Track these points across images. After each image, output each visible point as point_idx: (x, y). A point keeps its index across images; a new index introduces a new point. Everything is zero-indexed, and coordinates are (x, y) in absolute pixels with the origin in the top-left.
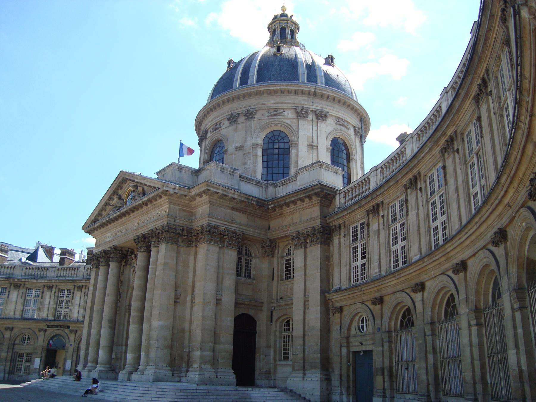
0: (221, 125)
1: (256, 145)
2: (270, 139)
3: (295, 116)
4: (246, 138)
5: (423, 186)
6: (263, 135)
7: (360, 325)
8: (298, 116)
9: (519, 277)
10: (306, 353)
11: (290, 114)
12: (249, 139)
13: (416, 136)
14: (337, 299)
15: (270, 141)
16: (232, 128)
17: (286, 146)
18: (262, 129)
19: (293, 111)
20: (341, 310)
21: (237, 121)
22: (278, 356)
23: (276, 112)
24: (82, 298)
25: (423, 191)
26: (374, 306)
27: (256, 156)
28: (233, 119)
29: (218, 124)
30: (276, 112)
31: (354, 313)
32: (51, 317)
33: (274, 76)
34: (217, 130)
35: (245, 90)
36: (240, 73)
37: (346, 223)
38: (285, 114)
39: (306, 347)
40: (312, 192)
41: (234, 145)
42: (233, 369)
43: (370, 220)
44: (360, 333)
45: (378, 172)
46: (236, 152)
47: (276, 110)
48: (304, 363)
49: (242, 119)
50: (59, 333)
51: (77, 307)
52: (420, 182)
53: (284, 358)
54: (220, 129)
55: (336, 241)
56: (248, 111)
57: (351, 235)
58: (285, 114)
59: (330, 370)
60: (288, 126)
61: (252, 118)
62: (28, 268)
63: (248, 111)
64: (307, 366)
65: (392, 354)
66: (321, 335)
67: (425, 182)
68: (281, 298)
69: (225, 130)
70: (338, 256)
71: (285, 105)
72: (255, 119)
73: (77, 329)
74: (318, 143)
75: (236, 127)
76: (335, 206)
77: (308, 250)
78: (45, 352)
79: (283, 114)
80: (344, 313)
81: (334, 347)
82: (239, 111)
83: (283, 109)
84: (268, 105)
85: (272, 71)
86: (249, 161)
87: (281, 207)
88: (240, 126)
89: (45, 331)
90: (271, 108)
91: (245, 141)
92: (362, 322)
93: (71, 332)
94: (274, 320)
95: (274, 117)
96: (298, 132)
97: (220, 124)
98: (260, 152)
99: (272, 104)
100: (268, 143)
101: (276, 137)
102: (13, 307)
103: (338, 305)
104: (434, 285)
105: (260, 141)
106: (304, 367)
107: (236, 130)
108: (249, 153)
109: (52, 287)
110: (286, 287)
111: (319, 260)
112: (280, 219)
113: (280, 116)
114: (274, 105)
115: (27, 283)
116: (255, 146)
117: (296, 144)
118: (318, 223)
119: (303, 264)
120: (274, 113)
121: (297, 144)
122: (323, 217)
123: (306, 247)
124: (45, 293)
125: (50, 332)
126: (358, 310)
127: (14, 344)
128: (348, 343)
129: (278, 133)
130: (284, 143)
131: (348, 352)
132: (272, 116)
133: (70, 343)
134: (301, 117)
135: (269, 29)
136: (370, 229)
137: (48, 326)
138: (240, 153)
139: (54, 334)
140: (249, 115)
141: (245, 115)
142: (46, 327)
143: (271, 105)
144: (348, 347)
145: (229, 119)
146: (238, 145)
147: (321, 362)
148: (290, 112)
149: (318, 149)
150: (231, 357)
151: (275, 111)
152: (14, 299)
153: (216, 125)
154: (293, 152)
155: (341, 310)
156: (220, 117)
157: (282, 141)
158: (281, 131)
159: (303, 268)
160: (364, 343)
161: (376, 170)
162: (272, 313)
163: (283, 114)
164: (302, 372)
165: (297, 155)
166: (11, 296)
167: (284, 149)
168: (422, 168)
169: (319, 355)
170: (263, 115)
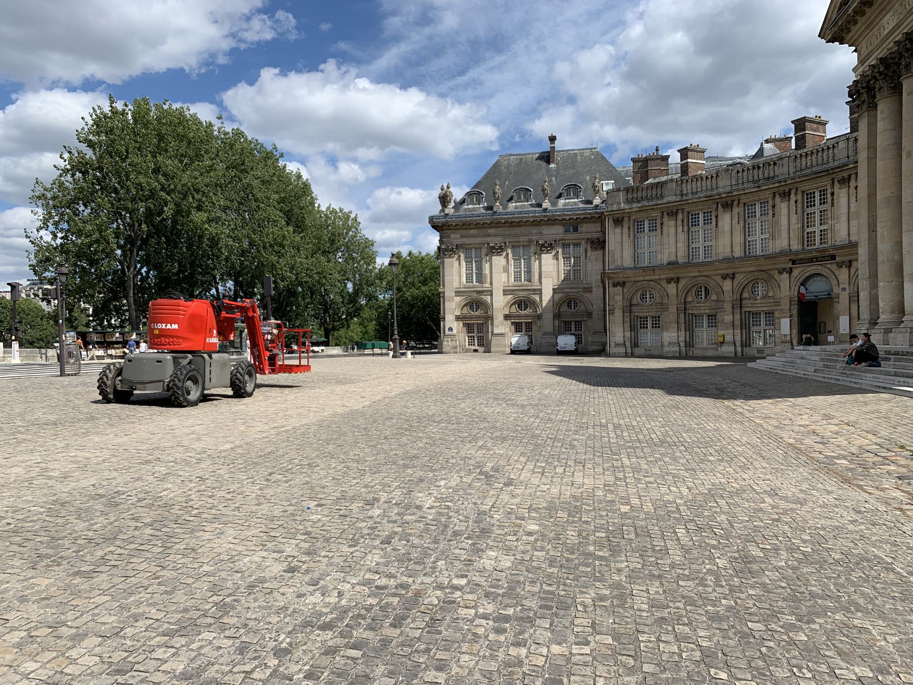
32: (795, 246)
51: (844, 218)
89: (790, 271)
93: (840, 266)
115: (743, 197)
137: (794, 262)
139: (808, 274)
152: (727, 228)
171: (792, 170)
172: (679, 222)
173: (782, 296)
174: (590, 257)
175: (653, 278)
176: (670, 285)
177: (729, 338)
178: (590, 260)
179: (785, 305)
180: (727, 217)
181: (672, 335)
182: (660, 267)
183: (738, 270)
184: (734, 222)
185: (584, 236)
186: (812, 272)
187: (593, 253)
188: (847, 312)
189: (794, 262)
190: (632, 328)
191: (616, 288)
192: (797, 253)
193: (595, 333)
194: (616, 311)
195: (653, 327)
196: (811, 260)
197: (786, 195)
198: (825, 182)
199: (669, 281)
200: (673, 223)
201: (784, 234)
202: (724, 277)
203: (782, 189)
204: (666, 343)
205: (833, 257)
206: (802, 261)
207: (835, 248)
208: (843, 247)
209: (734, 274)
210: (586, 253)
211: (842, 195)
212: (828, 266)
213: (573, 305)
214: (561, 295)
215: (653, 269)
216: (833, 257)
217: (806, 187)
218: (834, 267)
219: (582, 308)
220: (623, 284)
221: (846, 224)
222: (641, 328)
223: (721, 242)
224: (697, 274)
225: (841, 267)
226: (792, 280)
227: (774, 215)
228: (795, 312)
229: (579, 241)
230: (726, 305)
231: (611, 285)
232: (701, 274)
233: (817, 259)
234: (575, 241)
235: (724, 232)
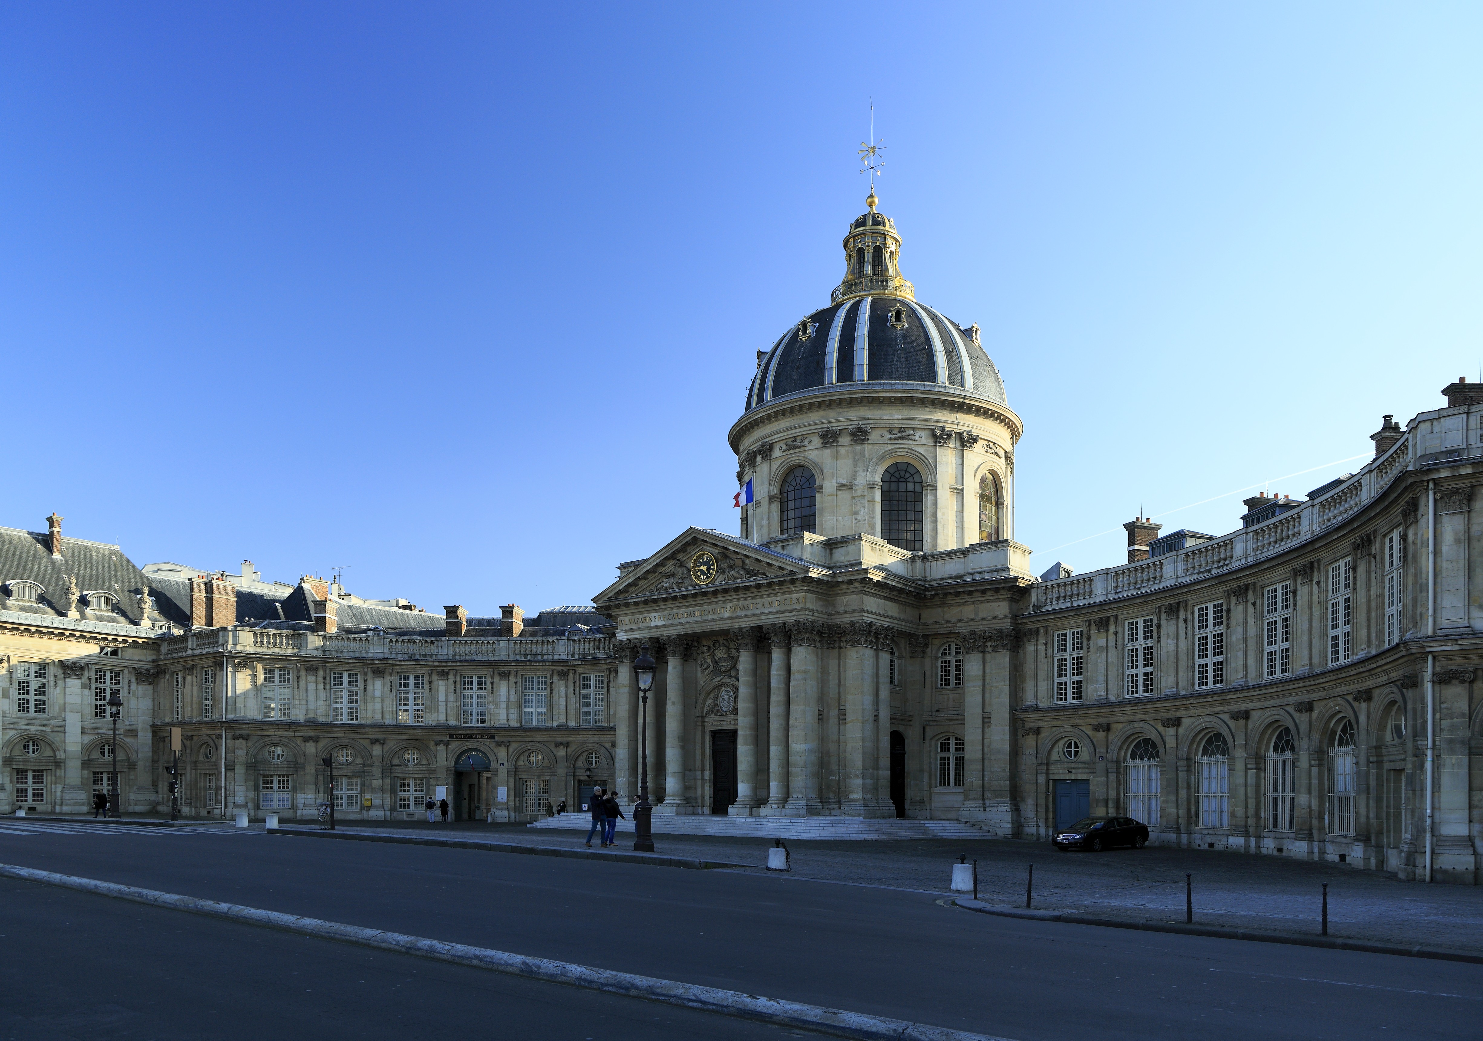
0: (806, 443)
1: (874, 484)
2: (892, 475)
3: (931, 442)
4: (856, 472)
5: (1189, 617)
6: (881, 469)
7: (1066, 750)
8: (935, 442)
9: (1321, 742)
10: (986, 779)
11: (923, 438)
12: (861, 474)
13: (1183, 556)
14: (1032, 720)
15: (893, 479)
16: (827, 452)
17: (918, 488)
18: (882, 458)
19: (927, 432)
20: (1037, 731)
21: (838, 442)
22: (933, 782)
23: (902, 434)
24: (512, 691)
25: (1189, 623)
26: (1094, 733)
27: (873, 501)
28: (829, 438)
29: (799, 439)
30: (902, 434)
31: (1059, 736)
32: (453, 722)
33: (897, 370)
34: (797, 450)
35: (846, 390)
36: (835, 354)
37: (1050, 629)
38: (917, 437)
39: (986, 773)
40: (1003, 585)
41: (834, 481)
42: (891, 798)
43: (1092, 632)
44: (1066, 760)
45: (1109, 576)
46: (840, 493)
47: (901, 430)
48: (983, 791)
49: (845, 440)
50: (475, 747)
51: (503, 705)
52: (1185, 611)
53: (941, 784)
54: (803, 449)
55: (1030, 648)
56: (859, 429)
57: (1056, 643)
58: (917, 437)
59: (1018, 799)
60: (921, 458)
61: (863, 440)
62: (394, 640)
63: (859, 429)
64: (988, 794)
65: (1120, 784)
66: (1010, 759)
67: (1193, 613)
68: (938, 711)
69: (815, 452)
70: (1033, 667)
71: (916, 422)
72: (869, 442)
73: (510, 739)
74: (963, 484)
75: (837, 452)
76: (1030, 603)
77: (988, 656)
78: (453, 776)
79: (913, 437)
80: (1042, 735)
81: (1027, 775)
82: (841, 425)
83: (913, 429)
84: (891, 422)
85: (893, 361)
86: (863, 510)
87: (946, 595)
88: (843, 451)
89: (447, 744)
90: (896, 425)
91: (854, 476)
92: (1070, 746)
93: (499, 744)
94: (928, 738)
95: (900, 442)
96: (936, 467)
97: (802, 441)
98: (878, 495)
99: (898, 419)
100: (890, 482)
101: (902, 473)
102: (378, 706)
103: (1033, 725)
104: (1196, 724)
105: (878, 479)
106: (983, 795)
107: (836, 456)
108: (863, 496)
109: (447, 674)
110: (946, 697)
111: (1008, 670)
112: (939, 610)
113: (909, 439)
114: (901, 422)
115: (398, 667)
116: (871, 485)
117: (933, 486)
118: (1006, 625)
119: (981, 673)
120: (900, 435)
121: (934, 487)
122: (1015, 617)
123: (985, 652)
124: (435, 683)
125: (456, 745)
126: (1067, 734)
127: (392, 765)
128: (1047, 769)
129: (912, 471)
130: (914, 482)
131: (1048, 780)
132: (896, 439)
133: (500, 762)
134: (940, 443)
135: (845, 245)
136: (1091, 643)
137: (452, 736)
138: (846, 495)
139: (465, 748)
140: (860, 435)
141: (853, 434)
142: (448, 738)
143: (896, 422)
144: (1047, 774)
145: (822, 437)
146: (842, 481)
147: (1010, 790)
148: (923, 434)
149: (963, 494)
150: (889, 784)
151: (901, 432)
152: (378, 693)
153: (795, 441)
154: (928, 499)
155: (1037, 731)
156: (804, 429)
157: (911, 479)
158: (909, 464)
159: (981, 677)
160: (1073, 771)
161: (1107, 574)
162: (924, 728)
163: (913, 437)
164: (981, 801)
165: (935, 504)
166: (370, 688)
167: (914, 492)
168: (1191, 599)
169: (1008, 782)
170: (882, 436)
171: (451, 653)
172: (320, 679)
173: (438, 765)
174: (134, 691)
175: (286, 734)
176: (307, 744)
177: (377, 802)
178: (134, 695)
179: (442, 775)
180: (378, 683)
181: (309, 796)
182: (298, 724)
183: (390, 736)
184: (386, 689)
185: (128, 663)
186: (470, 747)
187: (140, 687)
188: (505, 784)
189: (452, 736)
190: (256, 788)
191: (237, 741)
192: (455, 728)
193: (140, 789)
194: (237, 767)
195: (279, 788)
196: (470, 736)
197: (443, 674)
198: (485, 671)
199: (306, 740)
200: (313, 678)
201: (442, 709)
202: (374, 742)
203: (440, 668)
204: (301, 806)
205: (493, 737)
206: (461, 736)
207: (497, 729)
208: (504, 729)
209: (385, 740)
210: (129, 686)
211: (502, 686)
212: (487, 743)
213: (31, 747)
214: (92, 737)
215: (289, 725)
216: (493, 737)
217: (467, 671)
218: (493, 745)
219: (48, 753)
220: (246, 738)
221: (505, 711)
222: (264, 787)
223: (370, 707)
224: (342, 735)
225: (500, 746)
226: (449, 751)
227: (430, 690)
228: (451, 780)
229: (121, 669)
230: (374, 769)
231: (229, 736)
232: (346, 735)
233: (476, 736)
234: (114, 668)
235: (373, 697)
